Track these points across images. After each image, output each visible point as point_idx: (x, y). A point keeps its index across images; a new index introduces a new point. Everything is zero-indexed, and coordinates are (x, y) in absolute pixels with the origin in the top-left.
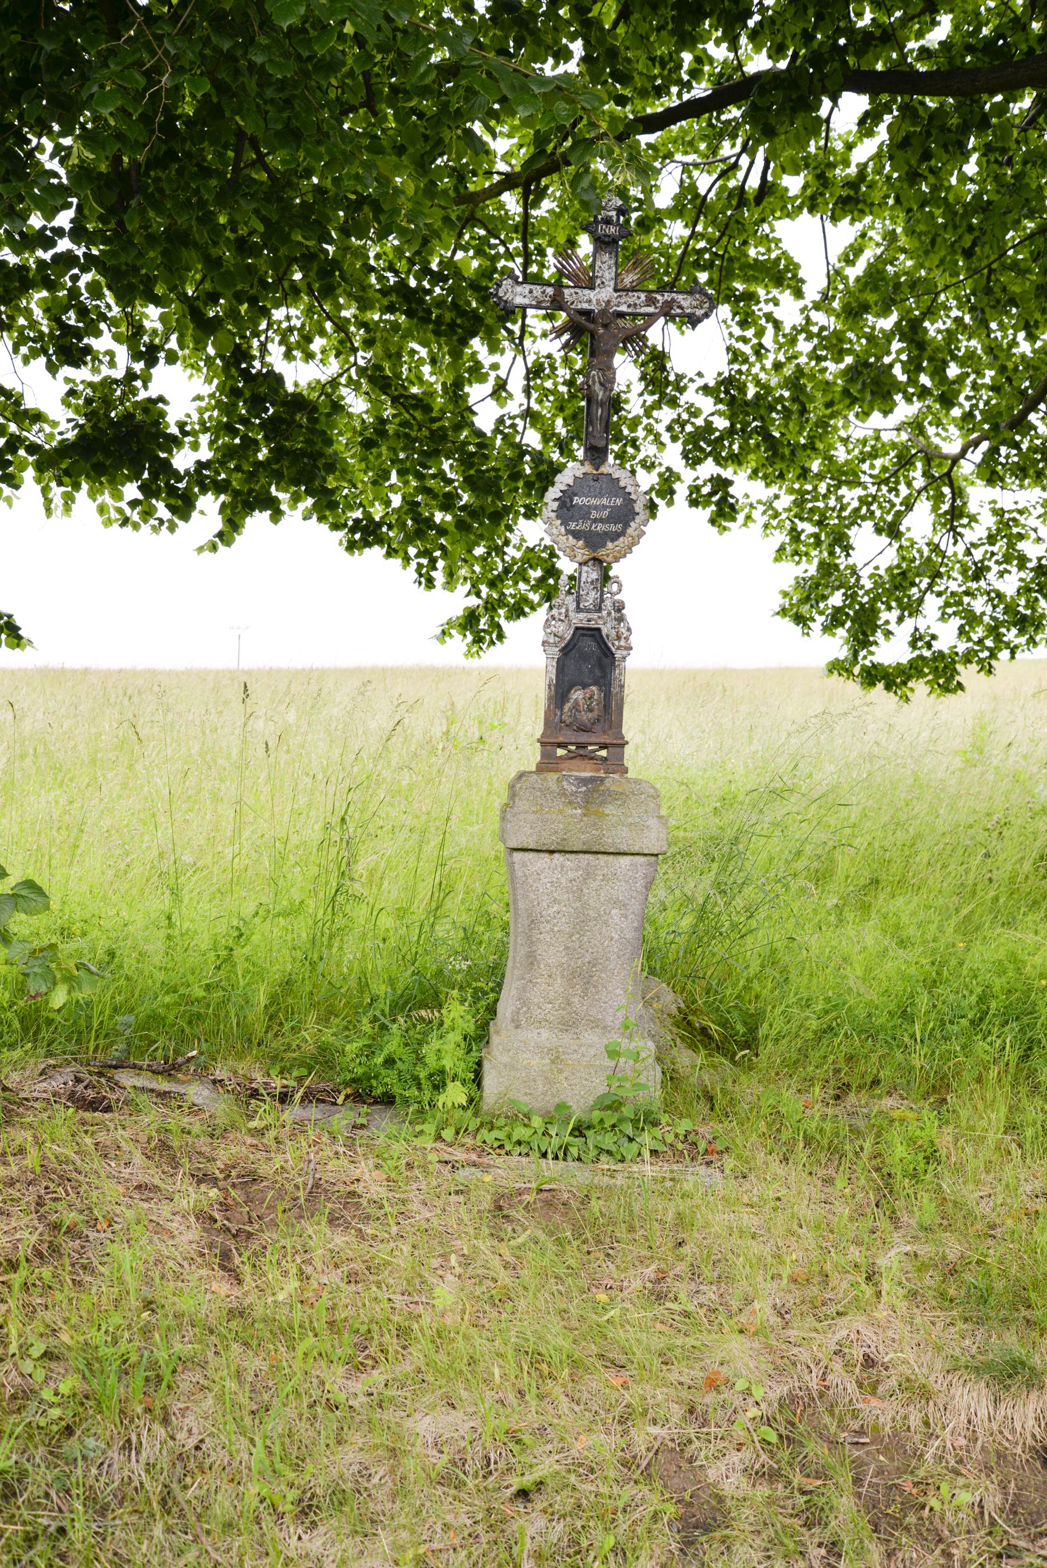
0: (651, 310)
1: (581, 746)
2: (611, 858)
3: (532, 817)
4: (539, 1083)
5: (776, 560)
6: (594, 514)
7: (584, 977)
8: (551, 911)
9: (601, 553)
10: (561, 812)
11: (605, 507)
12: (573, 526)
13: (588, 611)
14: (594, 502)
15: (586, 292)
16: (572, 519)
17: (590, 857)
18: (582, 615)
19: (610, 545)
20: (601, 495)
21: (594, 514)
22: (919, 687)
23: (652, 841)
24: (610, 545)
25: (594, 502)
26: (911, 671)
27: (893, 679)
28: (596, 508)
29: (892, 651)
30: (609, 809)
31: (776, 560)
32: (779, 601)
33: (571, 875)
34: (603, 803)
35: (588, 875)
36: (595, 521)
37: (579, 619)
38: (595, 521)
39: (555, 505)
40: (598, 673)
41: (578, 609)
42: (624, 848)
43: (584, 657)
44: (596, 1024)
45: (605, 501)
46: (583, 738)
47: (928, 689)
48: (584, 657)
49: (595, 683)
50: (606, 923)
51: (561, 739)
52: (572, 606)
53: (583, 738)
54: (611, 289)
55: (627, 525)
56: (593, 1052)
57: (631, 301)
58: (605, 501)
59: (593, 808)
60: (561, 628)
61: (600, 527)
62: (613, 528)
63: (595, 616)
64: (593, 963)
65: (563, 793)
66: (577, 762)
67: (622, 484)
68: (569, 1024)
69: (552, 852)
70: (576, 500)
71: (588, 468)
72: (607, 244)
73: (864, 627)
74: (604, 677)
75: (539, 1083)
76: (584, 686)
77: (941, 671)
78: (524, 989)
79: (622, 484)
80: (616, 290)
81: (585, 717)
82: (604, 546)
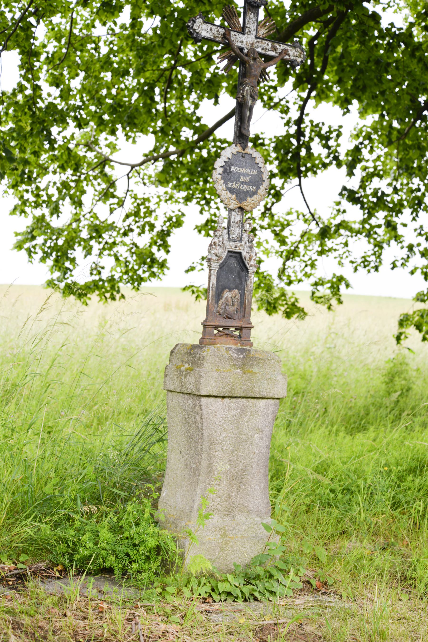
0: (273, 53)
1: (226, 328)
2: (255, 401)
3: (216, 374)
4: (217, 551)
5: (11, 214)
6: (242, 179)
7: (238, 479)
8: (222, 436)
9: (244, 204)
10: (230, 371)
11: (248, 175)
12: (230, 185)
13: (235, 241)
14: (242, 171)
15: (241, 35)
16: (229, 180)
17: (243, 400)
18: (231, 243)
19: (249, 199)
20: (245, 167)
21: (242, 179)
22: (94, 297)
23: (280, 390)
24: (249, 199)
25: (242, 171)
26: (95, 286)
27: (80, 292)
28: (243, 175)
29: (81, 275)
30: (255, 369)
31: (11, 214)
32: (14, 240)
33: (233, 412)
34: (252, 365)
35: (243, 413)
36: (242, 183)
37: (231, 246)
38: (242, 183)
39: (220, 170)
40: (238, 281)
41: (230, 240)
42: (265, 394)
43: (231, 271)
44: (245, 510)
45: (248, 171)
46: (228, 323)
47: (98, 298)
48: (231, 271)
49: (236, 288)
50: (251, 443)
51: (217, 323)
52: (226, 237)
53: (228, 323)
54: (253, 36)
55: (258, 188)
56: (244, 528)
57: (264, 46)
58: (248, 171)
59: (246, 368)
60: (219, 250)
61: (245, 188)
62: (252, 189)
63: (239, 244)
64: (243, 470)
65: (231, 359)
66: (224, 339)
67: (257, 161)
68: (229, 511)
69: (223, 397)
70: (233, 169)
71: (239, 148)
72: (253, 7)
73: (61, 257)
74: (241, 284)
75: (217, 551)
76: (230, 290)
77: (108, 289)
78: (205, 488)
79: (257, 161)
80: (256, 38)
81: (231, 309)
82: (246, 199)
